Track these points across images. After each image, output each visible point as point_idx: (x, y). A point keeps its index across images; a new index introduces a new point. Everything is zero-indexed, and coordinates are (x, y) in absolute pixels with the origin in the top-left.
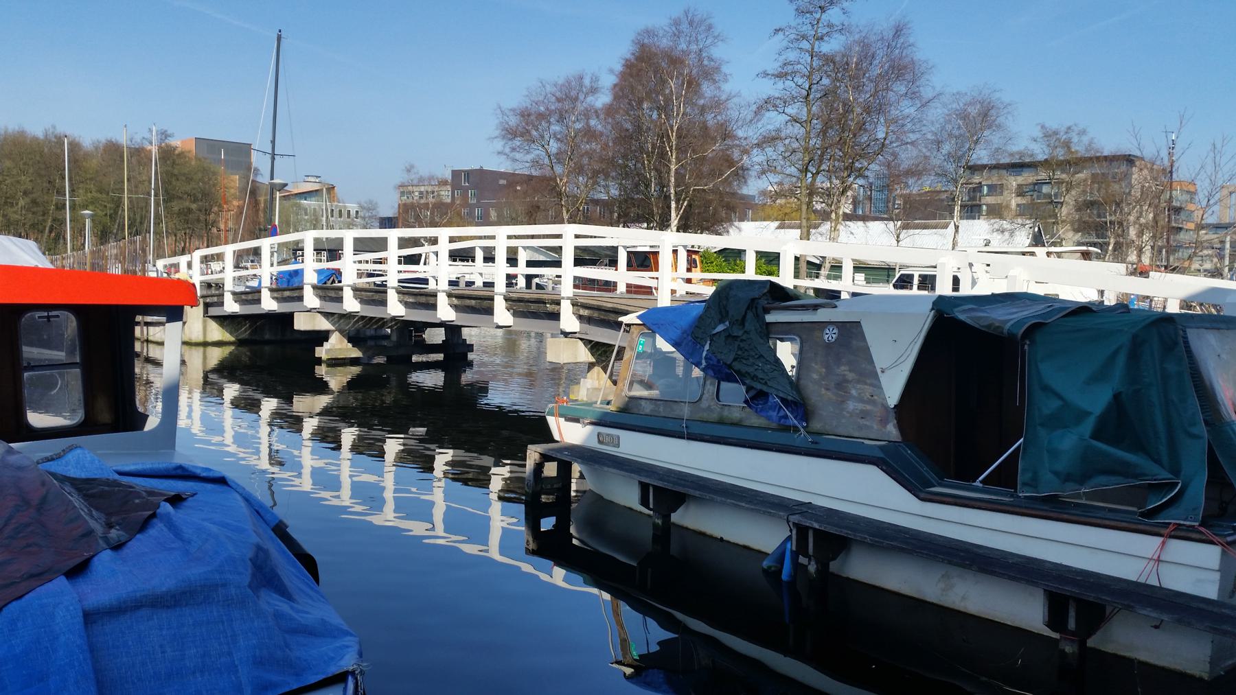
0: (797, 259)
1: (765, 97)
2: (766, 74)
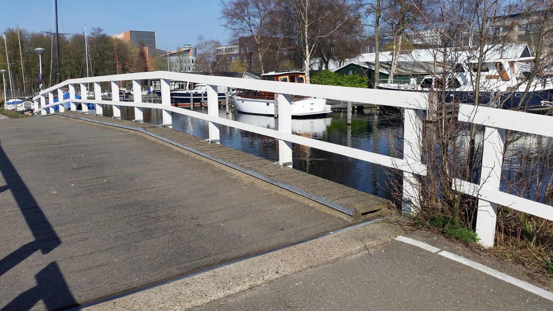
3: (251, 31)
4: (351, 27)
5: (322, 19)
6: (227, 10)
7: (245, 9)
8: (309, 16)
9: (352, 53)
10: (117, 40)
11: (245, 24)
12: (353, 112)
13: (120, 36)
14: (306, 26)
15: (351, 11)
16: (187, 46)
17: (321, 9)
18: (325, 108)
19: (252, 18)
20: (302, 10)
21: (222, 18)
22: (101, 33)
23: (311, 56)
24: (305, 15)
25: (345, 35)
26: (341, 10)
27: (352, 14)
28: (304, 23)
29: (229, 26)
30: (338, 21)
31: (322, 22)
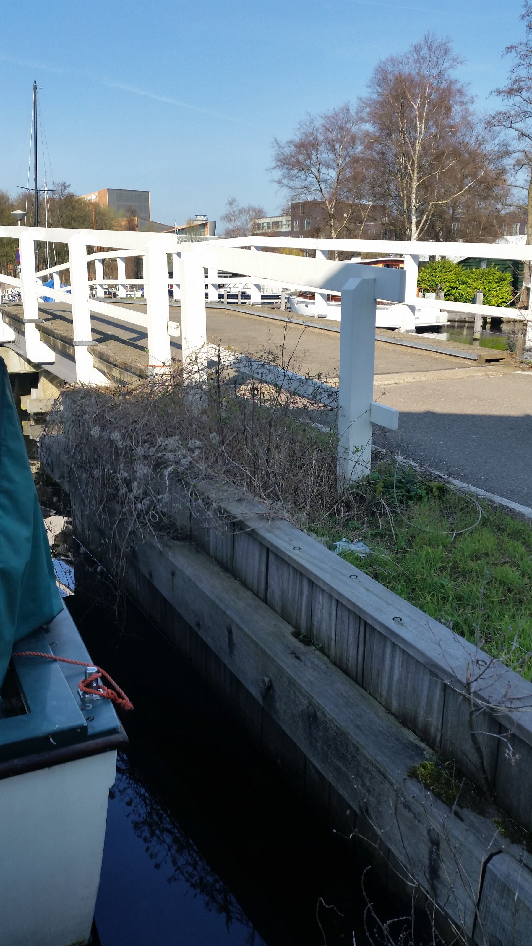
0: (219, 277)
1: (493, 113)
2: (499, 92)
3: (321, 191)
4: (489, 188)
5: (440, 174)
6: (283, 155)
7: (312, 154)
8: (420, 167)
9: (489, 234)
10: (91, 203)
11: (311, 179)
12: (484, 327)
13: (93, 197)
14: (415, 185)
15: (491, 161)
16: (201, 218)
17: (439, 156)
18: (438, 317)
19: (324, 170)
20: (410, 157)
21: (275, 168)
22: (66, 192)
23: (419, 234)
24: (413, 165)
25: (477, 202)
26: (474, 161)
27: (492, 167)
28: (411, 179)
29: (285, 181)
30: (467, 177)
31: (440, 179)
